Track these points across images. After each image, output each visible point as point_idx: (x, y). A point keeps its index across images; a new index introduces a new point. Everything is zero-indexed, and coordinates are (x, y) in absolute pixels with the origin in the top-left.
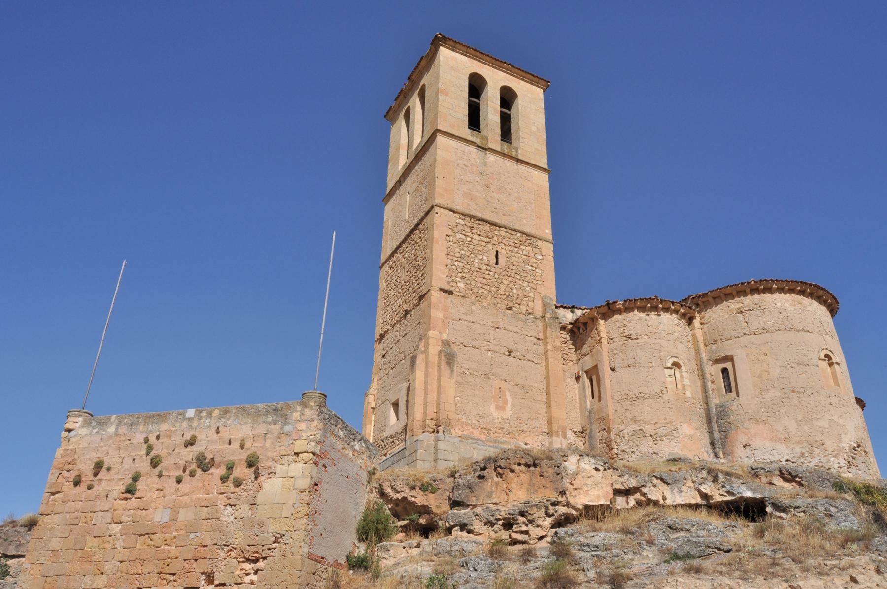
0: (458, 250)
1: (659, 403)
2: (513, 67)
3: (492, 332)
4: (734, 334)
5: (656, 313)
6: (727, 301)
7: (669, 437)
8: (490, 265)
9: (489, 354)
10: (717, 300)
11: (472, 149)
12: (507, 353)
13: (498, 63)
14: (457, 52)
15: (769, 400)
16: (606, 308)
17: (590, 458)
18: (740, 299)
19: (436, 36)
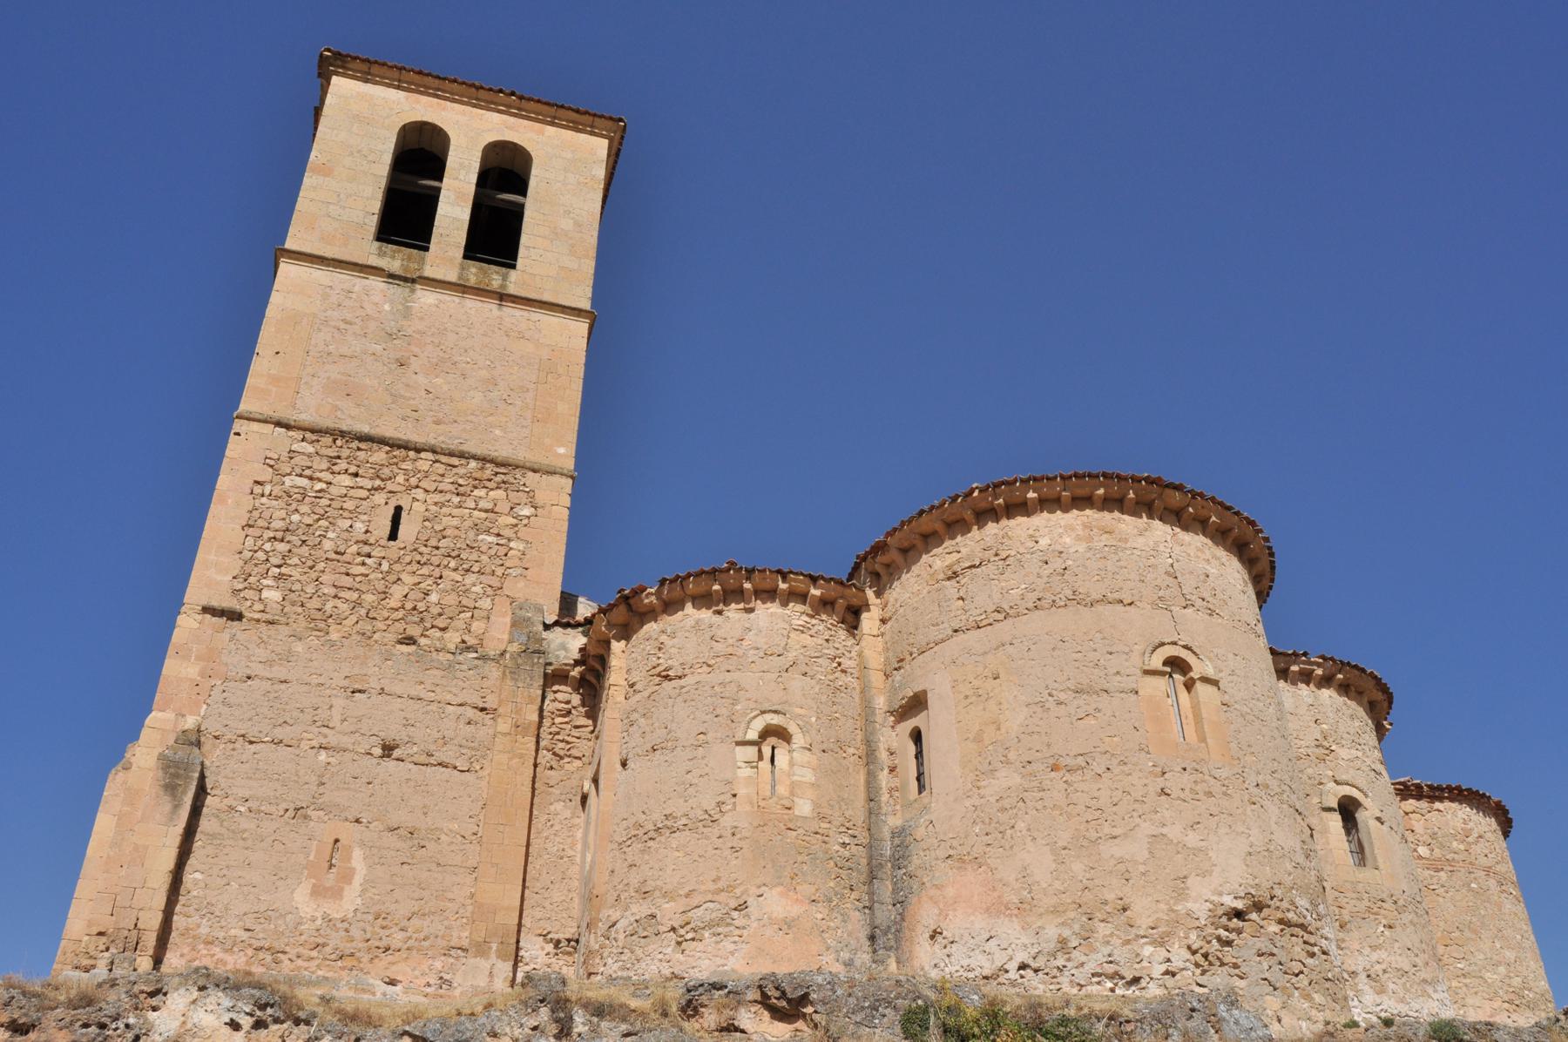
0: (283, 514)
1: (707, 838)
2: (521, 98)
3: (339, 702)
4: (934, 634)
5: (741, 606)
6: (928, 552)
7: (720, 930)
8: (372, 541)
9: (323, 756)
10: (911, 553)
11: (377, 283)
12: (378, 751)
13: (482, 93)
14: (376, 83)
15: (993, 800)
16: (622, 608)
17: (220, 994)
18: (953, 542)
19: (321, 55)
